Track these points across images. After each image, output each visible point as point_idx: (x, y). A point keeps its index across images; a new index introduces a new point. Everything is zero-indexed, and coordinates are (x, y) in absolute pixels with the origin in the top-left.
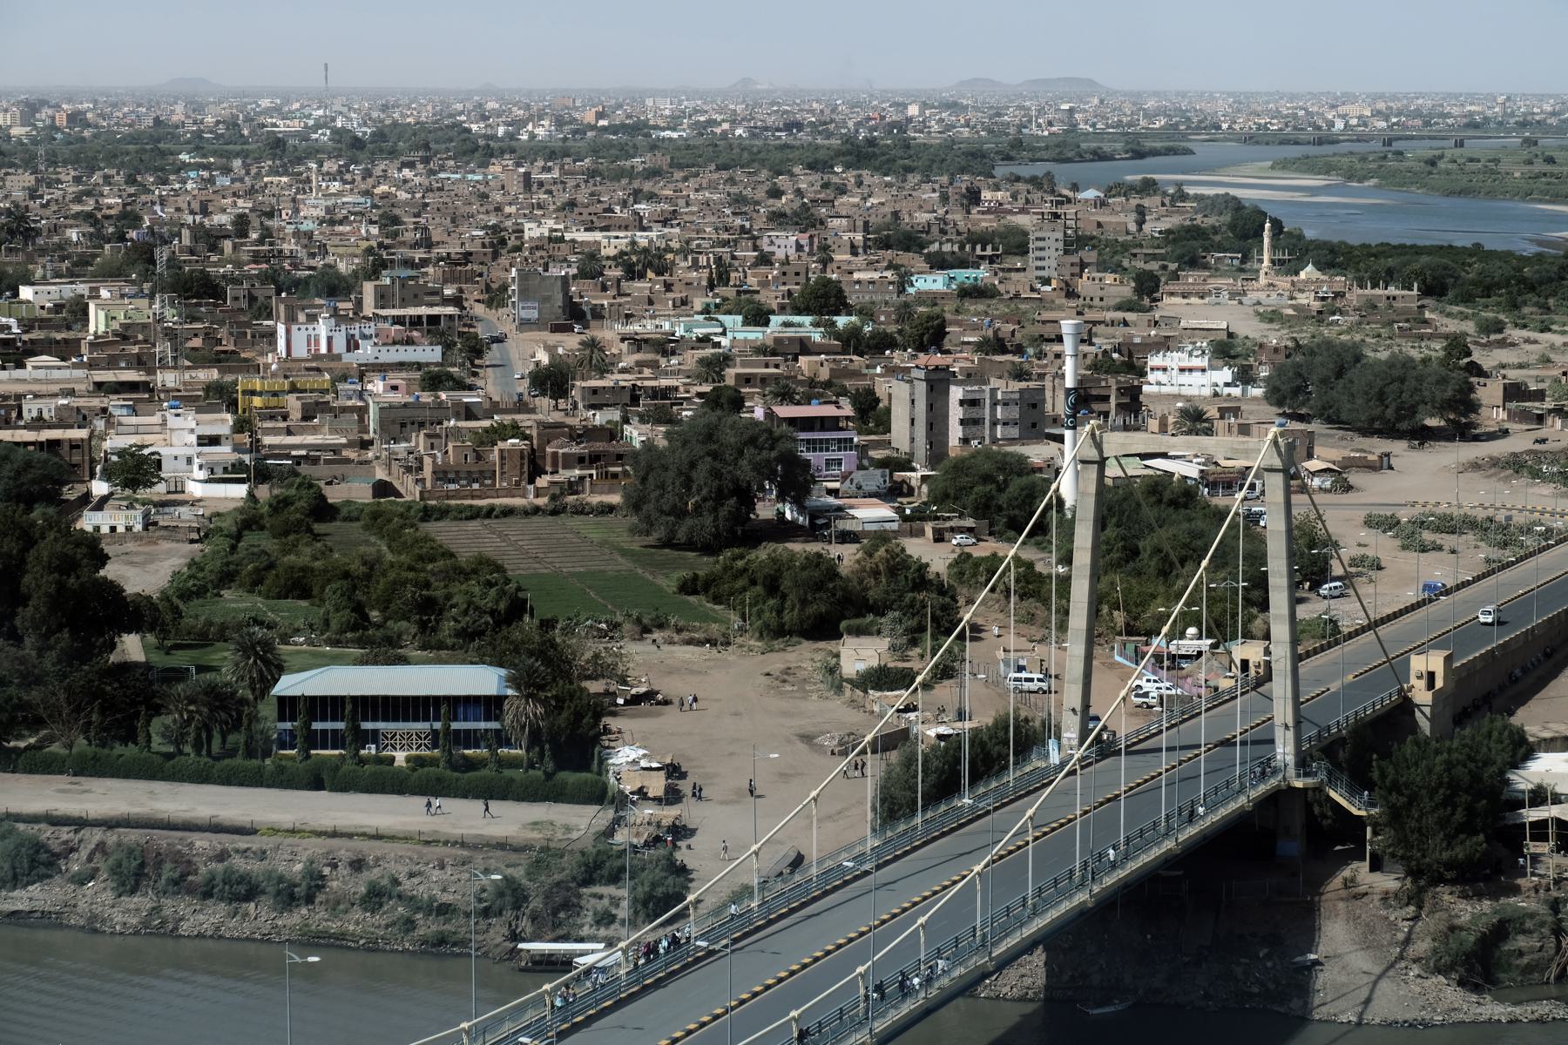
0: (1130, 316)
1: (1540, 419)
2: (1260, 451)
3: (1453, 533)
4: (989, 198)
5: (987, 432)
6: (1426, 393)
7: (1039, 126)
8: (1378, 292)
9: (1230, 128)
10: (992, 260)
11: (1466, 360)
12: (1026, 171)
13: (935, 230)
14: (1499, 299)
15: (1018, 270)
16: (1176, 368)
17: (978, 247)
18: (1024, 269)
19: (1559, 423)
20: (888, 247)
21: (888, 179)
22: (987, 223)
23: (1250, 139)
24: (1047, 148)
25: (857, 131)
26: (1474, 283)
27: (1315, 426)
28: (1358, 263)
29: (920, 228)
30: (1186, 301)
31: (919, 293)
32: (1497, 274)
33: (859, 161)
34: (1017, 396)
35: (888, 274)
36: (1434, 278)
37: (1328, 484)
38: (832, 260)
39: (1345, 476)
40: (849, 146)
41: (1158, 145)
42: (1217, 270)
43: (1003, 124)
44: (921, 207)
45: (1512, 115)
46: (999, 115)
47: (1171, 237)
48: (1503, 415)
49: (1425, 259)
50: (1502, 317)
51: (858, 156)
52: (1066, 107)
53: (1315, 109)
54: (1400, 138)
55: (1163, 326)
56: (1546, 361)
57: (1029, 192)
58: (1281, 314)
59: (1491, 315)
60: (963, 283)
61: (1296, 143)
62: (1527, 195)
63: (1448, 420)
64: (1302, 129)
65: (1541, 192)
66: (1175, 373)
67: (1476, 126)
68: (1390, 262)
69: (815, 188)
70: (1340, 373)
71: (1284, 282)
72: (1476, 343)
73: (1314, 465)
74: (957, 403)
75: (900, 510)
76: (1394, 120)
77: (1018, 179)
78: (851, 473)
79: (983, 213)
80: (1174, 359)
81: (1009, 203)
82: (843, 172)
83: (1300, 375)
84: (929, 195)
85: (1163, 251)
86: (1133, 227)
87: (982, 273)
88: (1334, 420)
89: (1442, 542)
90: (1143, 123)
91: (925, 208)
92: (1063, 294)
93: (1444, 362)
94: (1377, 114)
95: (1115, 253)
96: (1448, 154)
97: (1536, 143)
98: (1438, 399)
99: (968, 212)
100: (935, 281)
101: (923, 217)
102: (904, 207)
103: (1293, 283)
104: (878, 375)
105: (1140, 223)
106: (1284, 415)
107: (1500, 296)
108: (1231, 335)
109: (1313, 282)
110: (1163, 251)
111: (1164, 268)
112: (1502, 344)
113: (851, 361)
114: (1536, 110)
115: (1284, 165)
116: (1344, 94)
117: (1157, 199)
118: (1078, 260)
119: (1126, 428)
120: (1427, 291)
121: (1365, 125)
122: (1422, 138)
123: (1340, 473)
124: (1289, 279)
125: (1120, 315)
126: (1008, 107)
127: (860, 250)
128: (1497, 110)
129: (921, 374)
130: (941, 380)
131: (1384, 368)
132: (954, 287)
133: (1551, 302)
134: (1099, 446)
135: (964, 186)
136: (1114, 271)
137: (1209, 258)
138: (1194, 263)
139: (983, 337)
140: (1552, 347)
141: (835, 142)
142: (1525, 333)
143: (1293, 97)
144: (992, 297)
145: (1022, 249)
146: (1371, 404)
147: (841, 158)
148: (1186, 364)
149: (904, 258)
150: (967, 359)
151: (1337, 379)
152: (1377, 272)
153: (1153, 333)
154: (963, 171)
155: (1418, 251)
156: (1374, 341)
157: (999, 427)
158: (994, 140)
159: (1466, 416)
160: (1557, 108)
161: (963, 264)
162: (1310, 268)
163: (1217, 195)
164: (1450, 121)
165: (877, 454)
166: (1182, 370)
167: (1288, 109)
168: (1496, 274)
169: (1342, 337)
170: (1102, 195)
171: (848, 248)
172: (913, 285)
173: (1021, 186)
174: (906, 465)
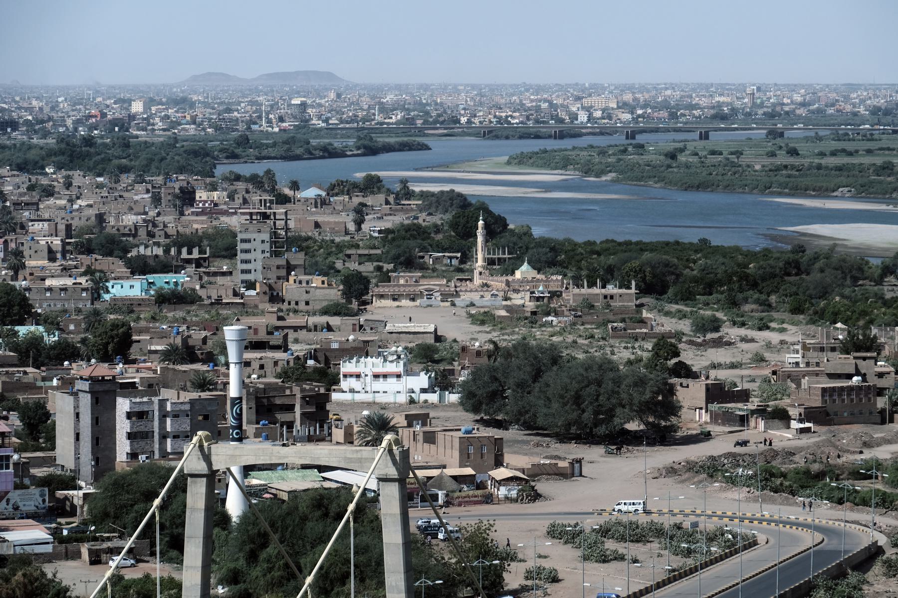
0: (335, 321)
1: (743, 420)
2: (374, 459)
3: (638, 541)
4: (204, 198)
5: (157, 446)
6: (624, 396)
7: (269, 122)
8: (596, 290)
9: (469, 122)
10: (198, 263)
11: (674, 361)
12: (245, 169)
13: (142, 233)
14: (719, 296)
15: (224, 274)
16: (370, 374)
17: (184, 250)
18: (231, 273)
19: (761, 424)
20: (89, 251)
21: (100, 179)
22: (197, 224)
23: (490, 133)
24: (274, 145)
25: (76, 129)
26: (696, 280)
27: (513, 433)
28: (579, 261)
29: (126, 231)
30: (397, 303)
31: (114, 299)
32: (720, 270)
33: (71, 161)
34: (187, 407)
35: (83, 280)
36: (654, 276)
37: (514, 494)
38: (23, 266)
39: (533, 484)
40: (63, 146)
41: (392, 140)
42: (434, 270)
43: (231, 120)
44: (131, 209)
45: (762, 105)
46: (229, 110)
47: (390, 236)
48: (706, 417)
49: (647, 256)
50: (720, 315)
51: (71, 156)
52: (296, 101)
53: (560, 101)
54: (643, 131)
55: (368, 330)
56: (759, 359)
57: (247, 192)
58: (493, 316)
59: (709, 313)
60: (162, 288)
61: (537, 137)
62: (766, 189)
63: (647, 424)
64: (543, 122)
65: (780, 185)
66: (368, 379)
67: (723, 118)
68: (612, 260)
69: (21, 190)
70: (537, 375)
71: (498, 283)
72: (691, 343)
73: (501, 473)
74: (124, 416)
75: (56, 533)
76: (640, 112)
77: (238, 178)
78: (7, 493)
79: (197, 214)
80: (369, 365)
81: (225, 203)
82: (54, 173)
83: (496, 379)
84: (141, 196)
85: (378, 252)
86: (352, 227)
87: (183, 279)
88: (531, 426)
89: (625, 551)
90: (378, 118)
91: (136, 210)
92: (267, 298)
93: (652, 365)
94: (624, 106)
95: (329, 254)
96: (691, 146)
97: (781, 135)
98: (636, 401)
99: (182, 214)
100: (132, 287)
101: (130, 219)
102: (111, 208)
103: (508, 283)
104: (53, 388)
105: (359, 223)
106: (481, 421)
107: (722, 293)
108: (438, 339)
109: (528, 282)
110: (378, 252)
111: (379, 269)
112: (719, 343)
113: (25, 373)
114: (786, 101)
115: (521, 160)
116: (592, 86)
117: (381, 197)
118: (284, 263)
119: (310, 439)
120: (646, 289)
121: (610, 118)
122: (667, 130)
123: (527, 481)
124: (504, 278)
125: (323, 319)
126: (239, 103)
127: (59, 256)
128: (746, 100)
129: (86, 386)
130: (106, 392)
131: (581, 371)
132: (152, 292)
133: (773, 298)
134: (207, 458)
135: (177, 186)
136: (325, 274)
137: (427, 257)
138: (409, 263)
139: (170, 345)
140: (769, 346)
141: (51, 141)
142: (743, 332)
143: (538, 89)
144: (192, 302)
145: (230, 252)
146: (567, 408)
147: (53, 158)
148: (380, 370)
149: (102, 262)
150: (149, 369)
151: (534, 381)
152: (595, 270)
153: (351, 338)
154: (181, 170)
155: (642, 247)
156: (586, 342)
157: (169, 441)
158: (220, 138)
159: (666, 419)
160: (808, 98)
161: (165, 268)
162: (525, 267)
163: (442, 192)
164: (697, 113)
165: (39, 472)
166: (376, 376)
167: (532, 101)
168: (719, 271)
169: (554, 339)
170: (324, 194)
171: (45, 253)
172: (108, 292)
173: (241, 186)
174: (70, 483)
